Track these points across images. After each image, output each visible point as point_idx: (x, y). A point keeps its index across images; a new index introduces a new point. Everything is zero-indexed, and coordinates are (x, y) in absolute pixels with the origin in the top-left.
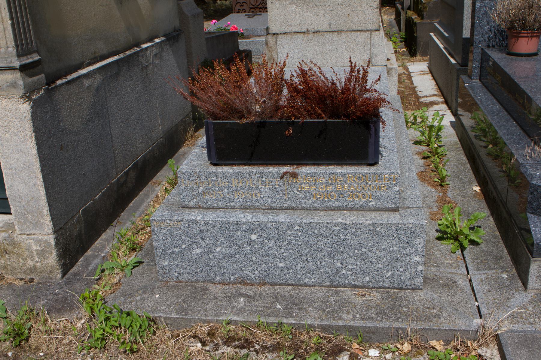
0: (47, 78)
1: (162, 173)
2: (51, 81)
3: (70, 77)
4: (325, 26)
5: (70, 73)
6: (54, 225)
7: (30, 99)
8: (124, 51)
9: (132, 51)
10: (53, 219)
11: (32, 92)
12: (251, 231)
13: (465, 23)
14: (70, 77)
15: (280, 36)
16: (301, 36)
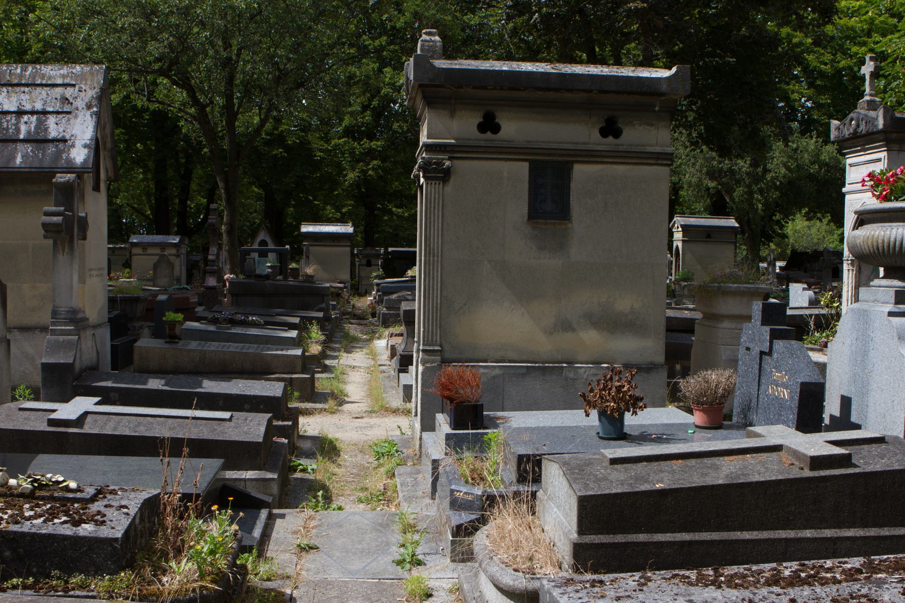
11: (427, 362)
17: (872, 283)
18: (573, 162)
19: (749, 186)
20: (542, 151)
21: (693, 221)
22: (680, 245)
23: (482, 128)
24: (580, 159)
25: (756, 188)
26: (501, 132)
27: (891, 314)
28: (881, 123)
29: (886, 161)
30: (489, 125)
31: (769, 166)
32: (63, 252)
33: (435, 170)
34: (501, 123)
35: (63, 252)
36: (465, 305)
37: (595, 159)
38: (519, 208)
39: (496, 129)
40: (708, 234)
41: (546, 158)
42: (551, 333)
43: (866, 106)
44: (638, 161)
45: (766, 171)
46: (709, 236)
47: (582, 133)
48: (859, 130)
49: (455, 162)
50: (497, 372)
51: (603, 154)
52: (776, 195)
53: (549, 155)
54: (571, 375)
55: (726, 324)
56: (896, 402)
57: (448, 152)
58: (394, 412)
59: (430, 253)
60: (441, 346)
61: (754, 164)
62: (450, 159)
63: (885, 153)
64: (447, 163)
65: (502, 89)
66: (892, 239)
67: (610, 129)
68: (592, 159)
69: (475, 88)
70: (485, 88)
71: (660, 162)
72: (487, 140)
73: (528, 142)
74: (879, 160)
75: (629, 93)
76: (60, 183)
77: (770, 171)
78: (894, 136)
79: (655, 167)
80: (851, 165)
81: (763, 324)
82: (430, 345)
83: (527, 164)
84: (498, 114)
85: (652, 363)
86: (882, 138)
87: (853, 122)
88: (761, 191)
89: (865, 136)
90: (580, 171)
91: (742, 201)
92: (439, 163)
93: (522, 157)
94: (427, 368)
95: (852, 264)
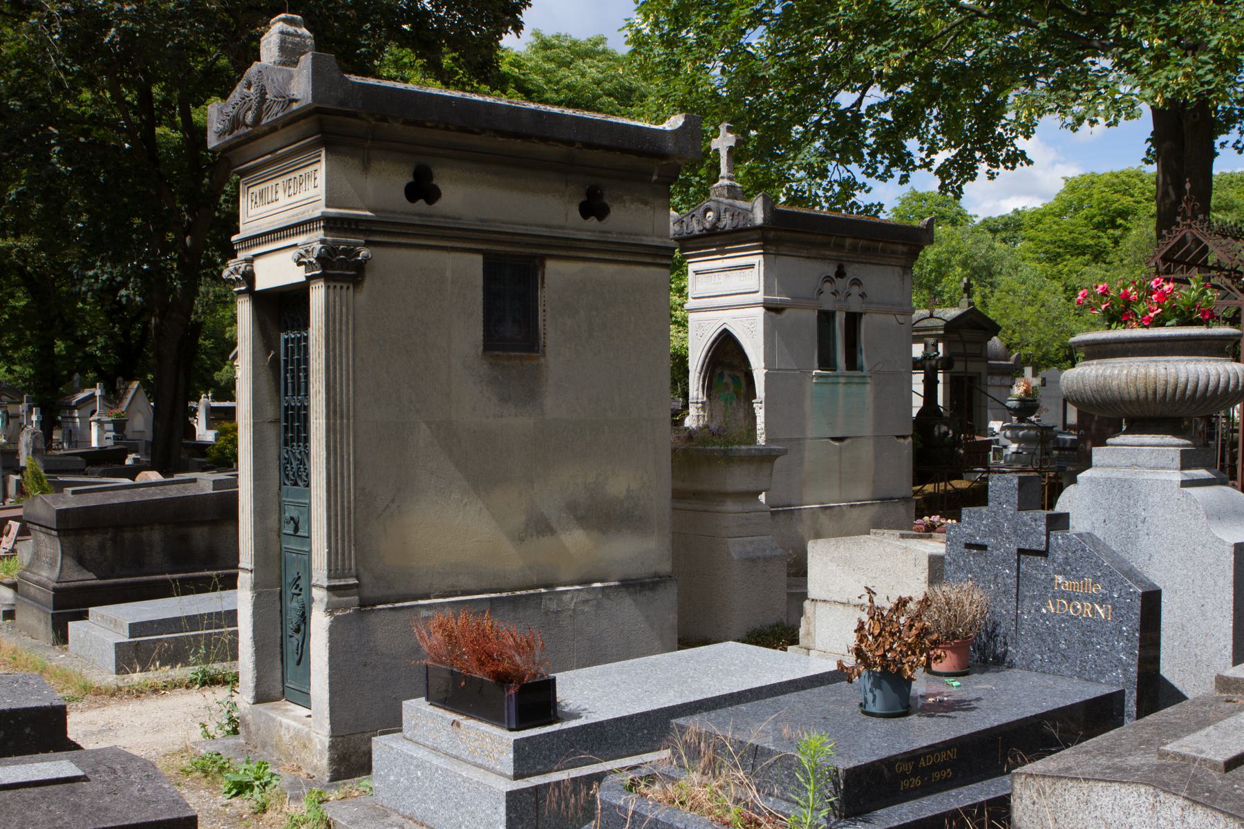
0: (360, 600)
1: (1071, 762)
2: (363, 604)
3: (397, 605)
5: (398, 601)
6: (332, 729)
7: (331, 614)
8: (512, 590)
9: (524, 592)
10: (331, 723)
11: (337, 609)
13: (122, 500)
14: (397, 605)
15: (819, 604)
16: (840, 607)
17: (1109, 441)
18: (543, 258)
20: (503, 237)
23: (413, 192)
24: (555, 253)
26: (436, 204)
27: (1184, 484)
28: (759, 217)
29: (762, 268)
30: (422, 189)
33: (344, 264)
34: (440, 186)
36: (393, 501)
37: (581, 254)
38: (468, 331)
39: (432, 195)
41: (510, 249)
42: (522, 540)
43: (725, 192)
44: (632, 259)
47: (547, 209)
48: (721, 225)
49: (379, 251)
51: (587, 245)
53: (512, 244)
54: (553, 606)
55: (730, 506)
56: (1209, 607)
57: (361, 232)
58: (113, 695)
59: (335, 412)
60: (357, 577)
62: (368, 244)
63: (761, 258)
64: (364, 252)
65: (447, 129)
66: (1172, 381)
67: (593, 207)
68: (572, 253)
69: (407, 123)
70: (422, 125)
71: (659, 261)
72: (420, 215)
73: (481, 221)
74: (751, 266)
75: (624, 151)
78: (772, 234)
79: (653, 269)
80: (696, 273)
81: (1023, 505)
82: (340, 578)
85: (656, 575)
86: (756, 237)
87: (710, 214)
89: (728, 232)
90: (557, 271)
92: (351, 252)
93: (473, 246)
94: (337, 619)
95: (703, 408)
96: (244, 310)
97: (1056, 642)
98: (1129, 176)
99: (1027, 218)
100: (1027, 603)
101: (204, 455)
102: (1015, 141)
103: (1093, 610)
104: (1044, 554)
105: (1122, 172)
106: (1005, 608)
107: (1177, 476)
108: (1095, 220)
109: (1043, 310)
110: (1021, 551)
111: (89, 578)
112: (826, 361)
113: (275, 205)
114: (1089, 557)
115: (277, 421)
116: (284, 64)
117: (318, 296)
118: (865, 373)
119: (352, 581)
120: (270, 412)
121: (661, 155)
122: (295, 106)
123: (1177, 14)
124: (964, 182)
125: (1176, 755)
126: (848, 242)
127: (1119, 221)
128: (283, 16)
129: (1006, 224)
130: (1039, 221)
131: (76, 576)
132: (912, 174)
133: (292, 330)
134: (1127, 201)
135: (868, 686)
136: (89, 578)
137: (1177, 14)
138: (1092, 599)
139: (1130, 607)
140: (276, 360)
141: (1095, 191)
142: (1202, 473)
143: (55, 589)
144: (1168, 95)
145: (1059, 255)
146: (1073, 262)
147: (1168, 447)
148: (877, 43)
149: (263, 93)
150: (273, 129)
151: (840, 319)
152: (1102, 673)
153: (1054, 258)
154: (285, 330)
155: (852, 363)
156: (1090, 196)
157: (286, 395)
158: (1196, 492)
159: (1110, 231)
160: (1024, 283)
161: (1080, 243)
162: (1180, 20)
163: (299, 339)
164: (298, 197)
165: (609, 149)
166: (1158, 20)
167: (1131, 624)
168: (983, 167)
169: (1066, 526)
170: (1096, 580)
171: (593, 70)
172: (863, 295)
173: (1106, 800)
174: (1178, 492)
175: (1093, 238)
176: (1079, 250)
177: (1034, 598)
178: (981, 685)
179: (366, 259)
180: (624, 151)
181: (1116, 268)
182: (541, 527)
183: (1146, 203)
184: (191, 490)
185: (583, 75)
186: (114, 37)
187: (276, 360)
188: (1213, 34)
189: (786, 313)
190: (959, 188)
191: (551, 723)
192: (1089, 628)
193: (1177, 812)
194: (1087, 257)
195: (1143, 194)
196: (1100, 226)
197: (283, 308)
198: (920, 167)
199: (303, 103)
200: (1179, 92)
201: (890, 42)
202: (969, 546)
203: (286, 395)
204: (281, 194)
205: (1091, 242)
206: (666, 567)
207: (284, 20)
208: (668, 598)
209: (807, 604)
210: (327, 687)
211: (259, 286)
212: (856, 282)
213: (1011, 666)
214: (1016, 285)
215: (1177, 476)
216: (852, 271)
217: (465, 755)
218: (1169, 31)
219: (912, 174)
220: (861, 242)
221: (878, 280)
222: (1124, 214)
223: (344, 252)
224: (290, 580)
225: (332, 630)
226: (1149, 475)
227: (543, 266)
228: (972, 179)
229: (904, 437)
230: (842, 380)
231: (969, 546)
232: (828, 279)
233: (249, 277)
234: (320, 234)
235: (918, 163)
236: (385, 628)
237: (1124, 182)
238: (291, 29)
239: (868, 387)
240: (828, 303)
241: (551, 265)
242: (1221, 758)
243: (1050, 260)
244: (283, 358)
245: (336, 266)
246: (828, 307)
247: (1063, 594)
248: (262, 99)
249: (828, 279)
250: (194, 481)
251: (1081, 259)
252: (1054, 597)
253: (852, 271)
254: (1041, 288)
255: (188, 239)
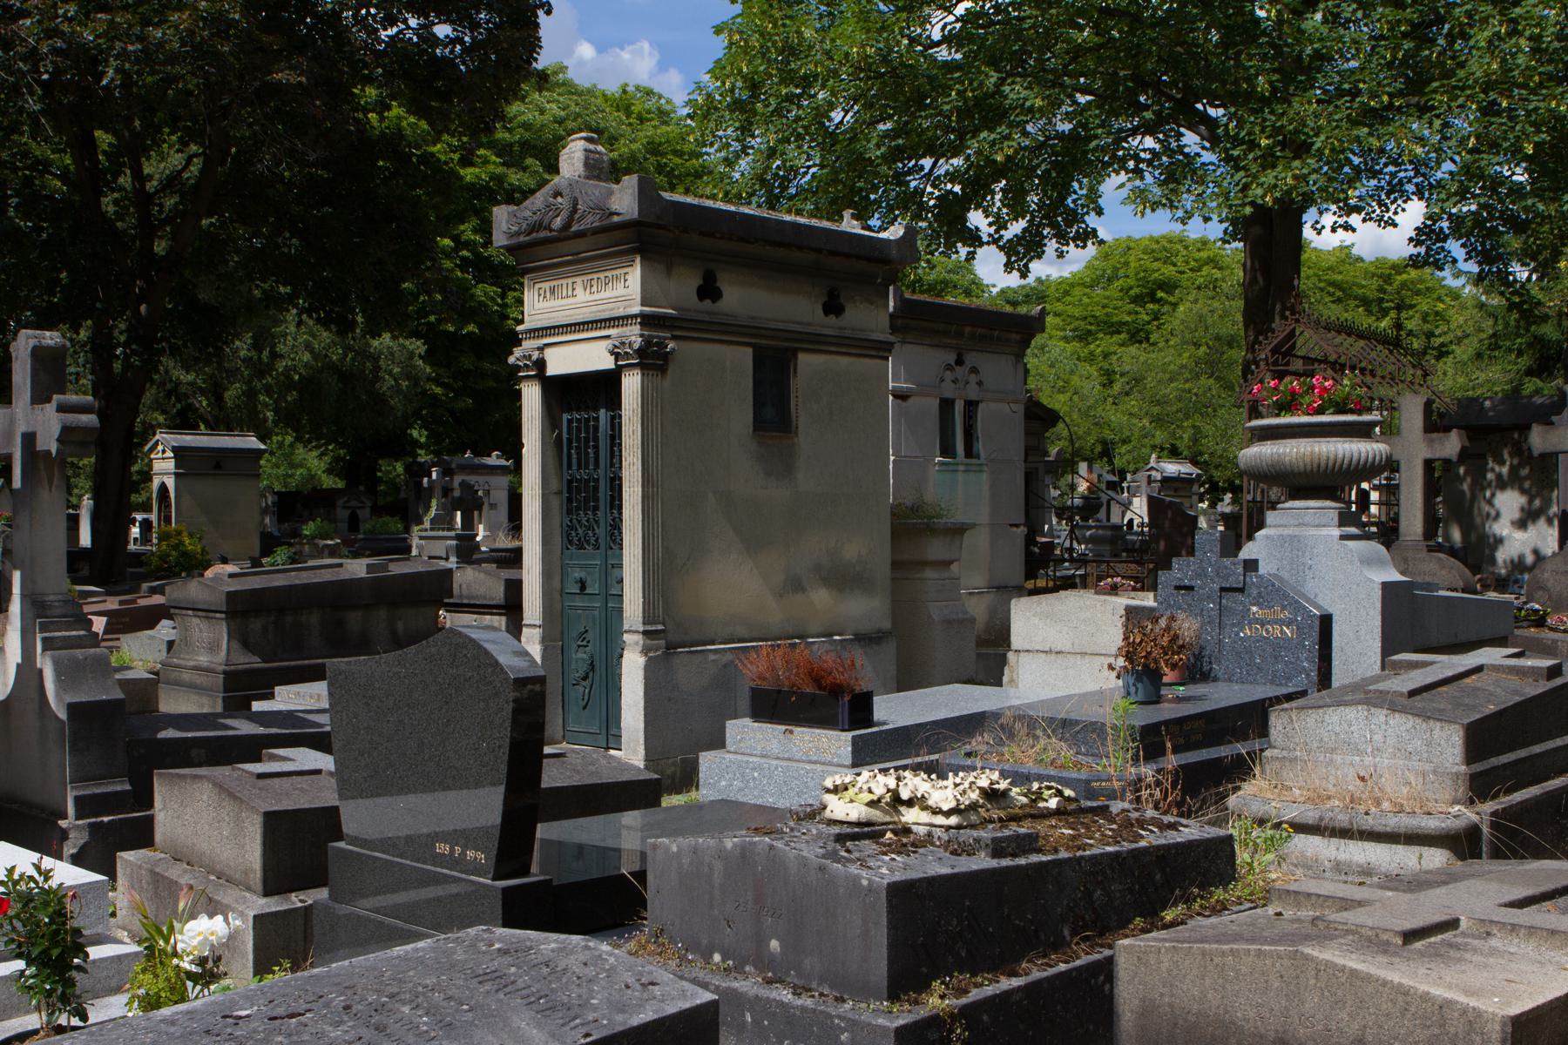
4: (1067, 647)
6: (646, 754)
12: (754, 769)
18: (795, 352)
19: (249, 383)
21: (188, 440)
22: (170, 483)
25: (259, 386)
27: (1343, 537)
30: (709, 291)
31: (280, 348)
32: (51, 483)
33: (657, 355)
35: (51, 483)
38: (742, 415)
40: (219, 462)
45: (275, 356)
46: (218, 466)
47: (795, 308)
50: (729, 657)
52: (292, 397)
55: (930, 573)
61: (257, 346)
62: (674, 338)
67: (833, 307)
72: (708, 313)
75: (859, 257)
76: (49, 347)
77: (281, 356)
78: (900, 322)
83: (750, 350)
84: (719, 275)
85: (879, 631)
88: (268, 390)
91: (238, 406)
96: (532, 397)
97: (1252, 658)
98: (1171, 242)
99: (1053, 289)
100: (1227, 630)
101: (141, 564)
102: (1086, 218)
103: (1282, 632)
104: (1241, 590)
105: (1163, 237)
106: (1210, 636)
107: (1336, 532)
108: (1132, 292)
109: (1076, 398)
110: (1223, 589)
111: (255, 662)
112: (947, 450)
113: (571, 300)
114: (1275, 593)
115: (560, 493)
116: (587, 177)
117: (631, 384)
118: (982, 460)
119: (660, 627)
120: (555, 485)
121: (886, 261)
122: (616, 219)
123: (1283, 114)
124: (1030, 260)
125: (1376, 691)
126: (968, 330)
127: (1160, 294)
128: (583, 134)
129: (1027, 296)
130: (1067, 293)
131: (242, 659)
132: (979, 251)
133: (578, 410)
134: (1168, 271)
135: (1131, 681)
136: (255, 662)
137: (1283, 114)
138: (1281, 622)
139: (1311, 627)
140: (559, 436)
141: (1132, 258)
142: (1353, 530)
143: (225, 672)
144: (1278, 195)
145: (1090, 333)
146: (1105, 343)
147: (1326, 510)
148: (991, 130)
149: (575, 203)
150: (580, 234)
151: (959, 407)
152: (1289, 679)
153: (1084, 337)
154: (569, 410)
155: (969, 453)
156: (1127, 264)
157: (569, 467)
158: (1351, 544)
159: (1150, 306)
160: (1052, 366)
161: (1115, 319)
162: (1285, 121)
163: (587, 420)
164: (602, 295)
165: (848, 256)
166: (1265, 120)
167: (1311, 642)
168: (1051, 246)
169: (1256, 570)
170: (1283, 608)
171: (554, 106)
172: (980, 384)
173: (1335, 718)
174: (1337, 544)
175: (1129, 313)
176: (1113, 328)
177: (1233, 625)
178: (1200, 689)
179: (673, 350)
180: (859, 257)
181: (1160, 350)
182: (795, 585)
183: (1190, 274)
184: (343, 575)
185: (542, 112)
186: (113, 80)
187: (559, 436)
188: (1317, 135)
189: (911, 401)
190: (1026, 266)
191: (509, 888)
192: (1279, 645)
193: (1382, 718)
194: (1123, 336)
195: (1187, 263)
196: (1137, 300)
197: (597, 390)
198: (988, 243)
199: (627, 217)
200: (1289, 192)
201: (1003, 129)
202: (1178, 588)
203: (569, 467)
204: (579, 290)
205: (1128, 319)
206: (887, 625)
207: (586, 139)
208: (889, 650)
209: (1010, 655)
210: (642, 718)
211: (551, 371)
212: (974, 370)
213: (1215, 679)
214: (1045, 368)
215: (1336, 532)
216: (971, 359)
217: (798, 756)
218: (1277, 131)
219: (979, 251)
220: (980, 331)
221: (993, 368)
222: (1169, 286)
223: (657, 344)
224: (575, 634)
225: (649, 670)
226: (1313, 531)
227: (796, 358)
228: (1040, 257)
229: (1017, 526)
230: (961, 468)
231: (1178, 588)
232: (949, 367)
233: (541, 364)
234: (636, 329)
235: (985, 239)
236: (690, 672)
237: (1165, 249)
238: (592, 147)
239: (985, 476)
240: (949, 391)
241: (803, 358)
242: (1405, 690)
243: (1080, 338)
244: (565, 436)
245: (651, 359)
246: (948, 395)
247: (1257, 621)
248: (575, 210)
249: (949, 367)
250: (340, 565)
251: (1115, 338)
252: (1250, 624)
253: (971, 359)
254: (1072, 372)
255: (143, 308)
